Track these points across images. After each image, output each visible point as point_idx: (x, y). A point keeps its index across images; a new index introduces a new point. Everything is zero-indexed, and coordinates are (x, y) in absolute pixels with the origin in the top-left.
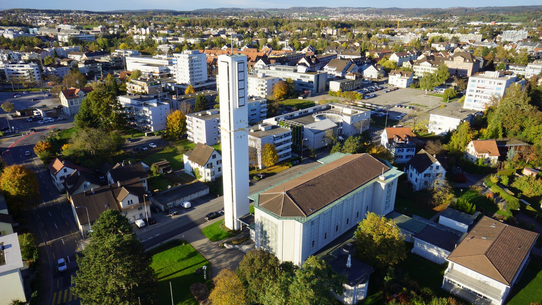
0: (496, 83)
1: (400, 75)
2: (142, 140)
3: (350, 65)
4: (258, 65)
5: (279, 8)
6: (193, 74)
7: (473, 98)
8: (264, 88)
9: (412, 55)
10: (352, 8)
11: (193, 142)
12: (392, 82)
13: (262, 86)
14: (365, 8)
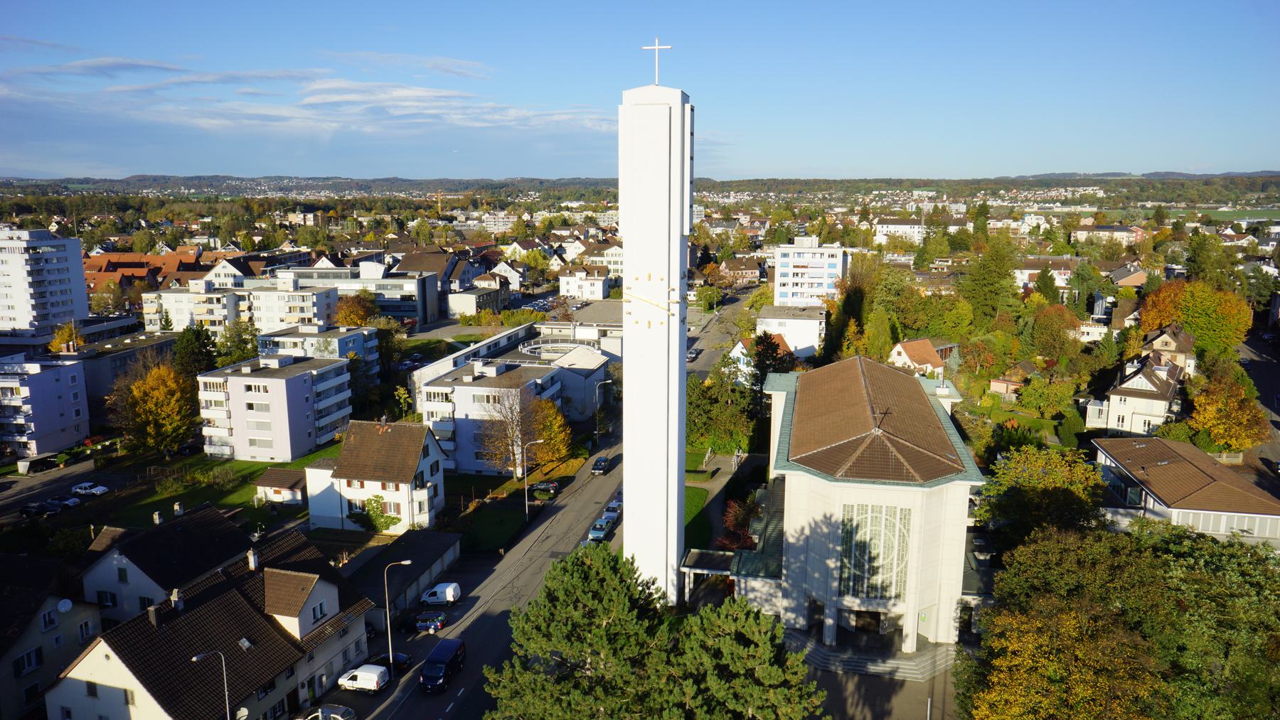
0: (826, 255)
1: (584, 274)
2: (16, 489)
3: (454, 265)
4: (218, 275)
5: (97, 177)
6: (43, 300)
7: (790, 289)
8: (308, 315)
9: (546, 247)
10: (297, 178)
11: (231, 459)
12: (568, 291)
13: (302, 310)
14: (327, 179)
